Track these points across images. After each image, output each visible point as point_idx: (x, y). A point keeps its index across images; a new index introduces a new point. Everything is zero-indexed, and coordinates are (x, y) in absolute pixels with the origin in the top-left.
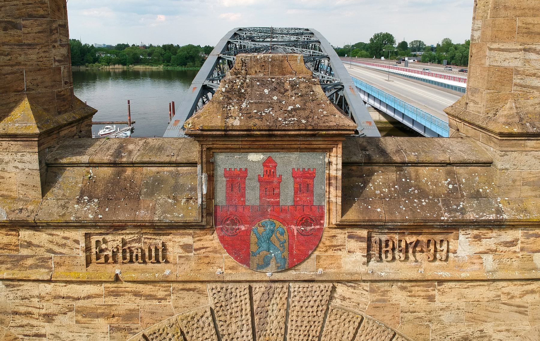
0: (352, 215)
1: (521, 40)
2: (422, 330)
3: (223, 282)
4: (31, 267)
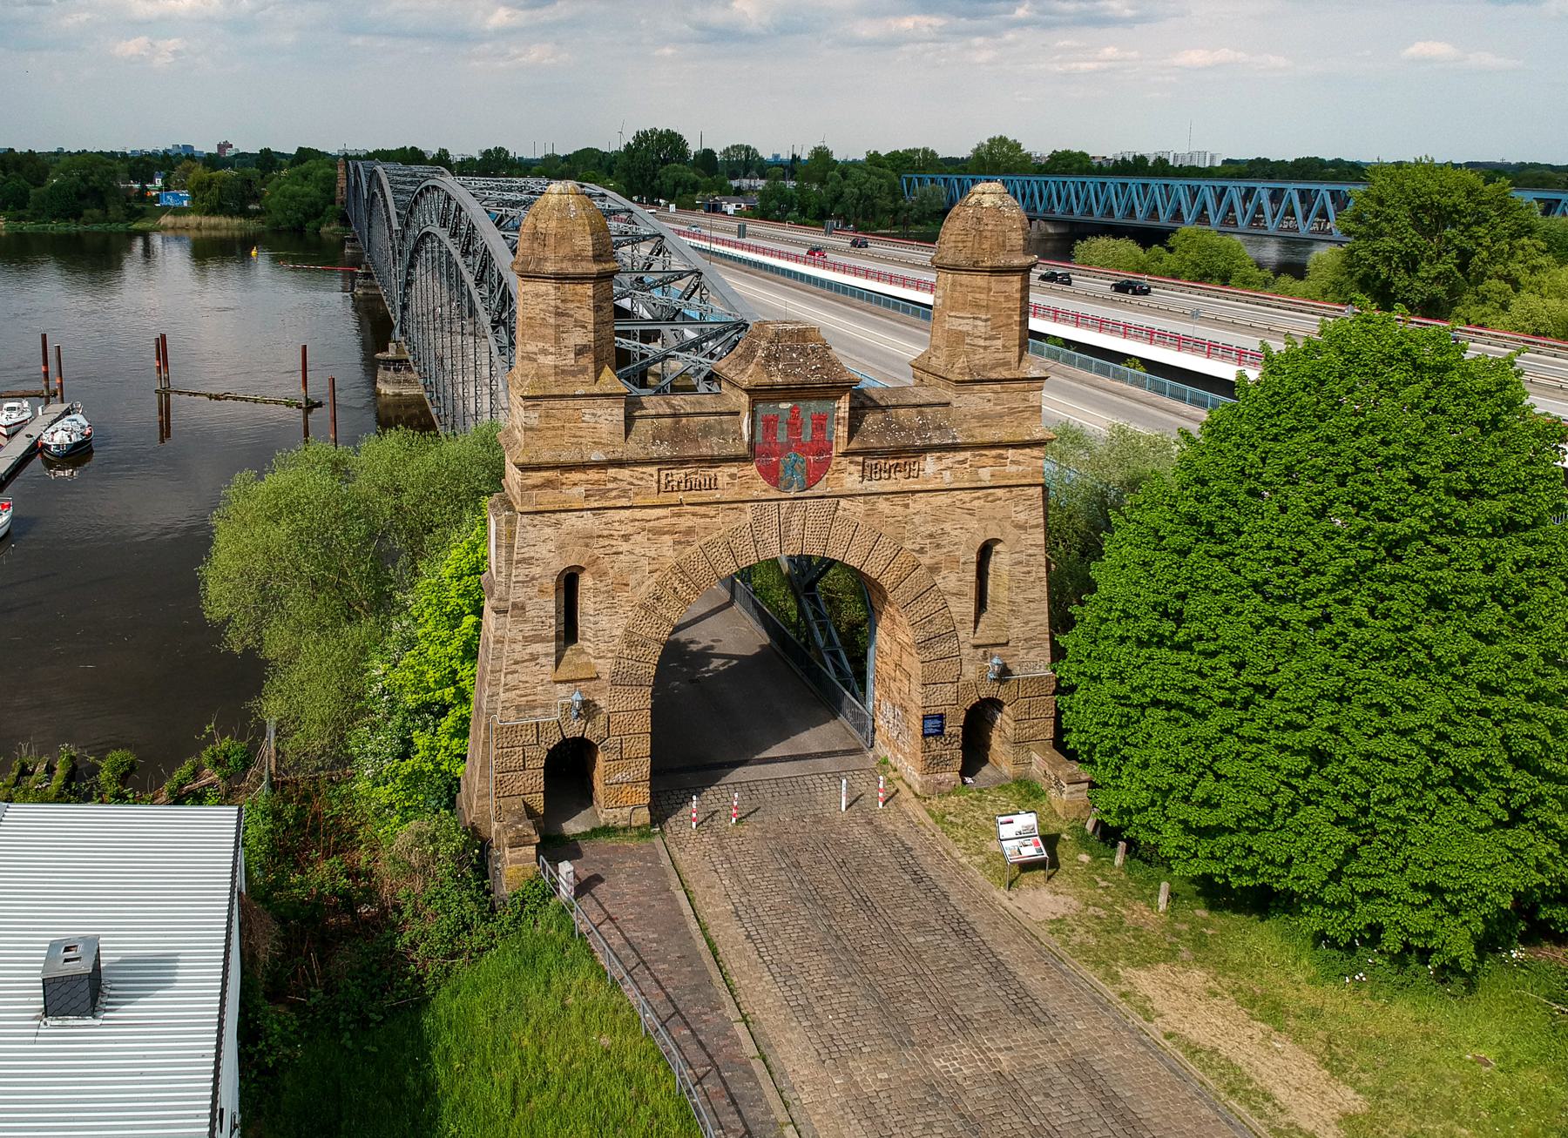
0: (854, 445)
2: (900, 530)
4: (615, 498)
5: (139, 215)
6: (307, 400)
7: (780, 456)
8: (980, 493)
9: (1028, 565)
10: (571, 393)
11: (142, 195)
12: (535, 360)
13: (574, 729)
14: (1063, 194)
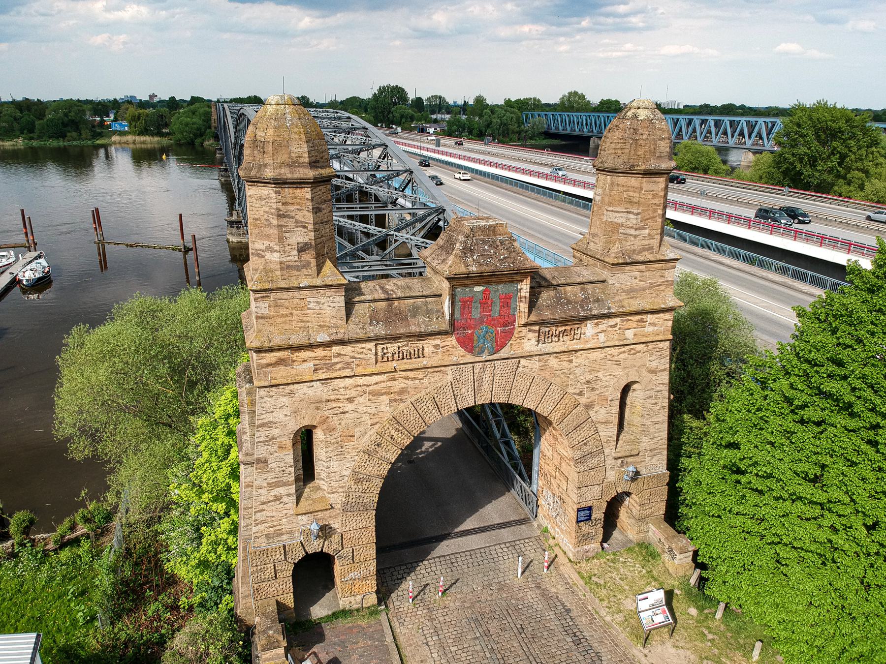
0: (533, 318)
1: (626, 206)
3: (457, 365)
4: (340, 369)
5: (100, 135)
6: (185, 247)
7: (474, 328)
8: (625, 349)
9: (656, 398)
10: (295, 286)
11: (102, 124)
12: (263, 257)
13: (314, 546)
14: (598, 123)
